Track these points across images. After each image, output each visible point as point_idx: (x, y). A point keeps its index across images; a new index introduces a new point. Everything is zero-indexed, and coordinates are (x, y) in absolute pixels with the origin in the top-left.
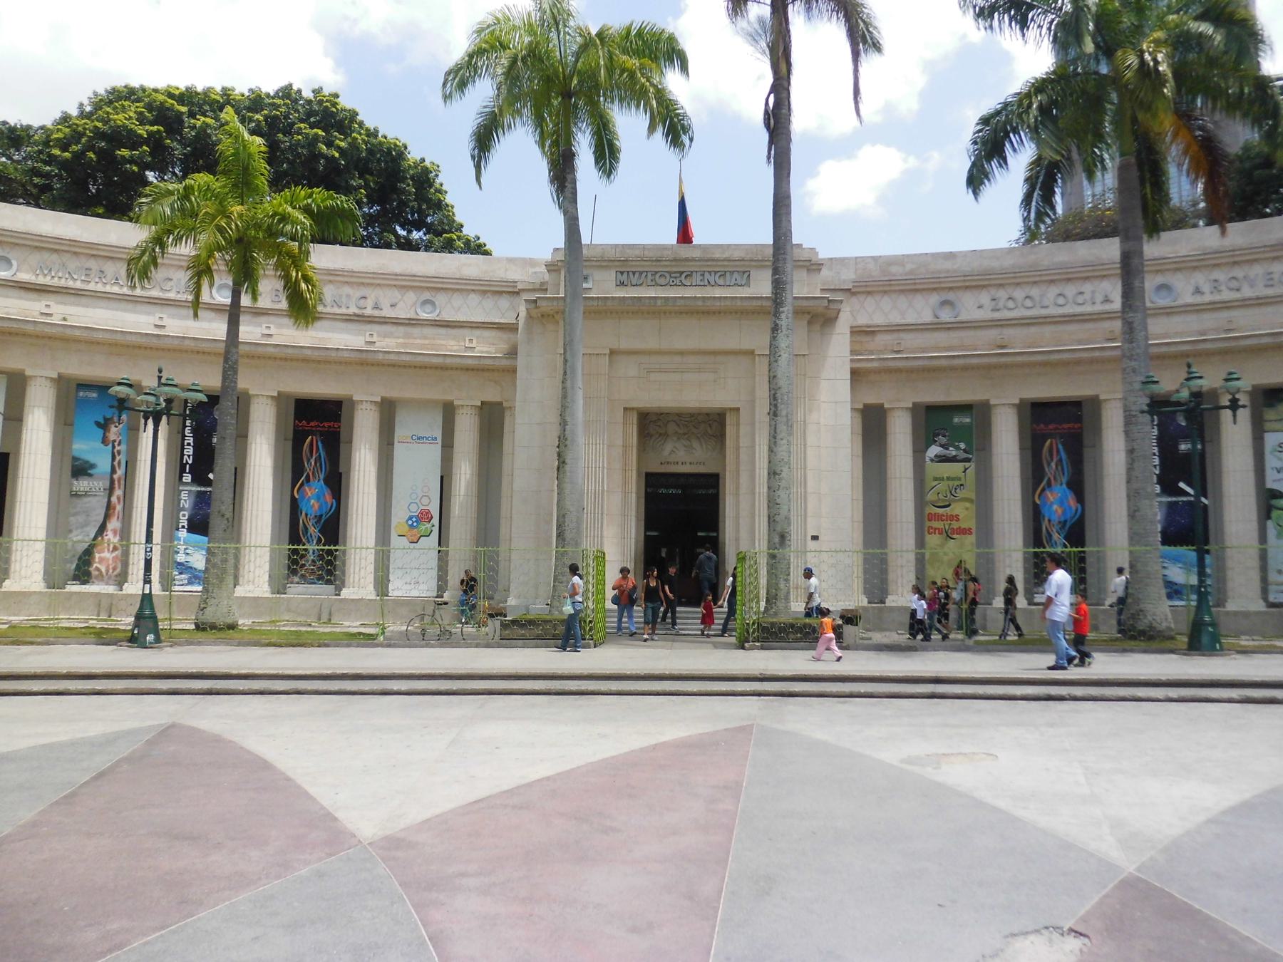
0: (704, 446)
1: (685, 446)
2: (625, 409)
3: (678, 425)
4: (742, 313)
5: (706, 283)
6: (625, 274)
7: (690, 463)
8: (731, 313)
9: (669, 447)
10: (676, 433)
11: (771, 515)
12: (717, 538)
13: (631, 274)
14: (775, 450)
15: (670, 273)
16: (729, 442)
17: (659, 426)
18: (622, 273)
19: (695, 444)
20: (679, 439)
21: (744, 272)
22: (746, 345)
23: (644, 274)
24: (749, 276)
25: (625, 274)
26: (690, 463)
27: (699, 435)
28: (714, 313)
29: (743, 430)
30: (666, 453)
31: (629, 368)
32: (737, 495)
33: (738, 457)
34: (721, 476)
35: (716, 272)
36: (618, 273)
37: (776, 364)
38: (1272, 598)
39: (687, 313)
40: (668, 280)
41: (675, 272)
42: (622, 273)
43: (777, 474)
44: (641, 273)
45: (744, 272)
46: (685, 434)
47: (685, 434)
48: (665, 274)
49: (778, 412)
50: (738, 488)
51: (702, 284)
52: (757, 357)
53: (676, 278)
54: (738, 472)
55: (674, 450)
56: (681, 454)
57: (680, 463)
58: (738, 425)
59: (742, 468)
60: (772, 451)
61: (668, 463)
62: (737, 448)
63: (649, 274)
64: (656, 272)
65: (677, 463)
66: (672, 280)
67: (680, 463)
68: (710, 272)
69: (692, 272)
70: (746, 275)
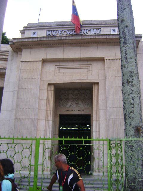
0: (84, 102)
1: (76, 103)
2: (49, 84)
3: (73, 95)
4: (98, 43)
6: (51, 31)
7: (78, 110)
8: (94, 43)
9: (69, 104)
10: (72, 98)
11: (127, 113)
12: (61, 125)
13: (53, 31)
14: (127, 65)
16: (94, 98)
17: (66, 96)
18: (49, 31)
19: (80, 103)
20: (73, 100)
21: (98, 29)
22: (101, 55)
25: (51, 31)
26: (78, 110)
27: (82, 99)
28: (86, 43)
29: (100, 91)
30: (68, 106)
31: (51, 67)
32: (98, 121)
33: (98, 104)
34: (91, 116)
35: (87, 29)
36: (48, 32)
37: (122, 14)
38: (12, 143)
39: (75, 44)
40: (67, 33)
41: (70, 30)
42: (49, 31)
43: (130, 82)
44: (57, 31)
45: (98, 29)
46: (76, 98)
47: (76, 98)
48: (67, 31)
49: (127, 41)
50: (99, 117)
52: (105, 60)
53: (70, 32)
54: (98, 110)
55: (72, 105)
56: (74, 107)
57: (74, 110)
58: (98, 90)
59: (101, 108)
60: (124, 67)
61: (69, 110)
62: (98, 100)
63: (60, 31)
64: (63, 30)
65: (73, 110)
66: (69, 33)
67: (74, 110)
69: (91, 29)
70: (99, 30)
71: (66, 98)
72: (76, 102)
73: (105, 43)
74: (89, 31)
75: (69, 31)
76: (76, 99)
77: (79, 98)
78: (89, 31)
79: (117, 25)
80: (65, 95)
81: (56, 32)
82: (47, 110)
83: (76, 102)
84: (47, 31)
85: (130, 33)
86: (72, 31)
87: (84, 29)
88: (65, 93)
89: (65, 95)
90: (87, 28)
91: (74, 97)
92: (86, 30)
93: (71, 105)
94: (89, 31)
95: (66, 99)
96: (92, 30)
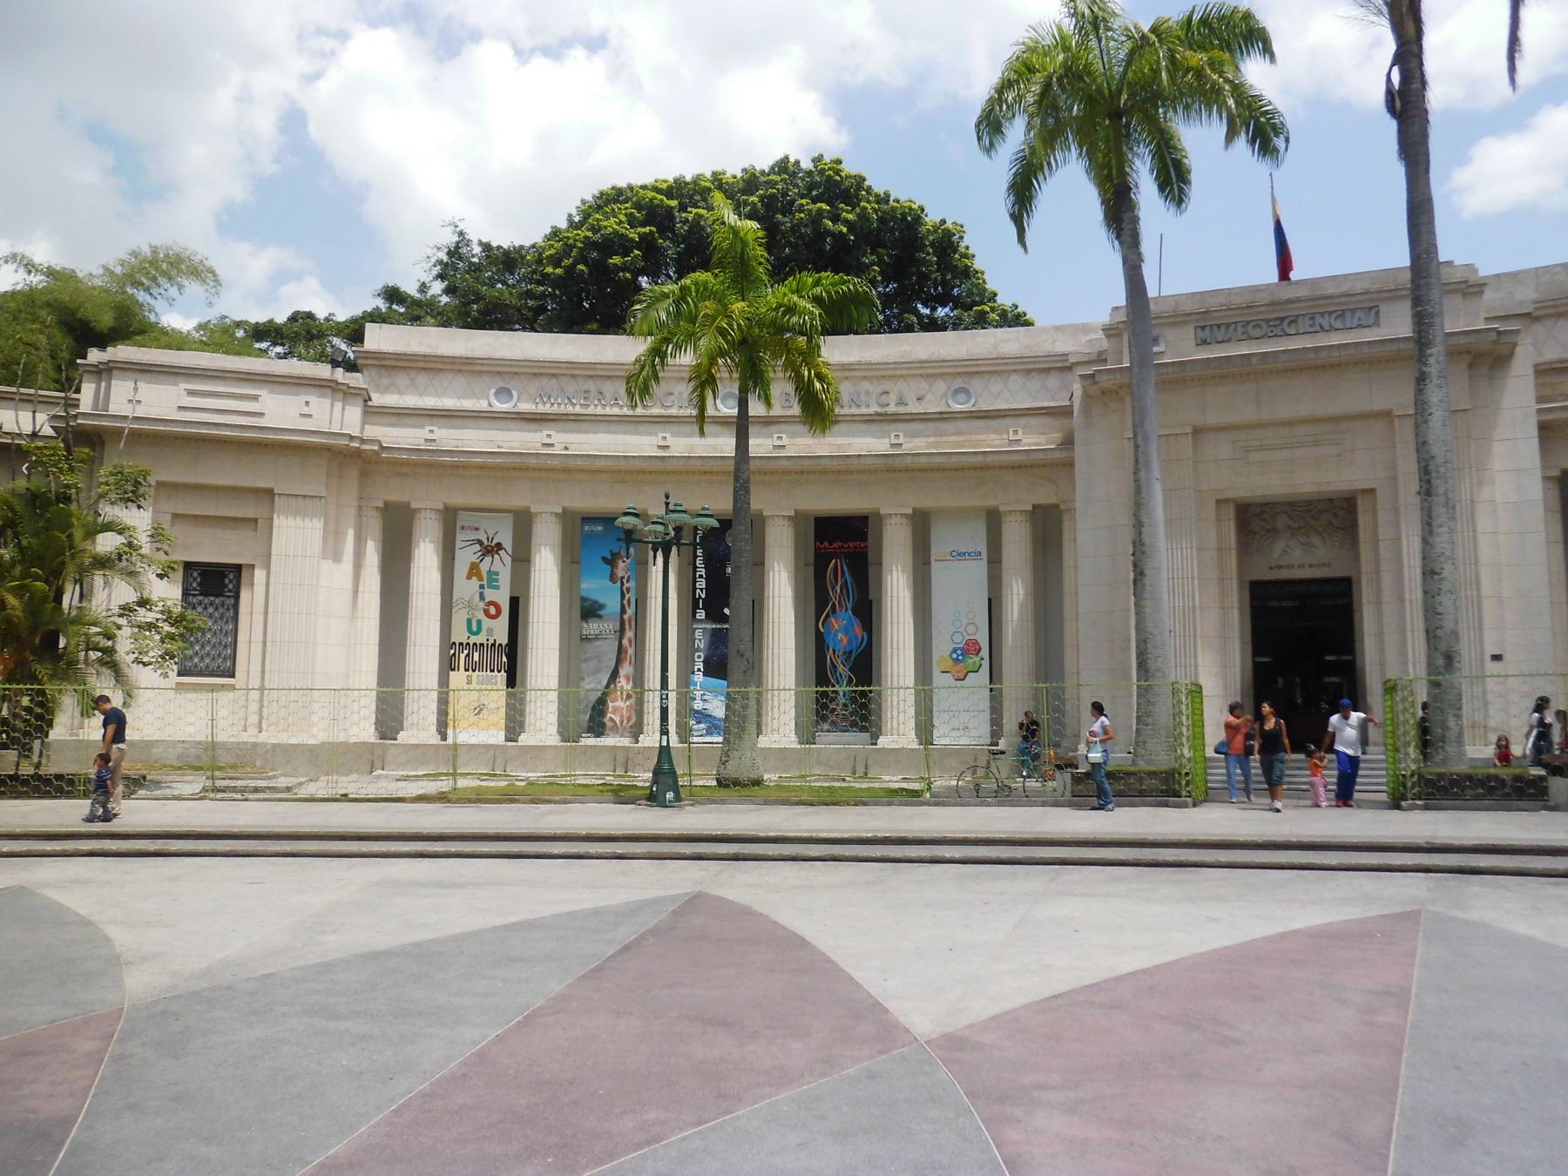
1: (1302, 544)
3: (1291, 518)
5: (1318, 329)
6: (1208, 329)
9: (1280, 545)
10: (1289, 527)
13: (1216, 330)
15: (1267, 321)
17: (1265, 520)
19: (1316, 540)
22: (1379, 404)
23: (1232, 327)
24: (1378, 312)
27: (1320, 529)
30: (1276, 554)
34: (1354, 580)
35: (1331, 313)
36: (1199, 330)
41: (1276, 319)
48: (1262, 323)
50: (1378, 594)
51: (1312, 330)
53: (1275, 326)
55: (1287, 549)
56: (1297, 555)
62: (1375, 543)
64: (1248, 323)
68: (1322, 314)
69: (1297, 316)
70: (1374, 311)
71: (1268, 527)
72: (1301, 540)
73: (1395, 360)
74: (1290, 323)
75: (1271, 323)
76: (1303, 531)
77: (1311, 527)
78: (1293, 325)
79: (1225, 778)
80: (1264, 517)
81: (1353, 317)
82: (1222, 580)
83: (1301, 540)
84: (1196, 327)
85: (490, 278)
86: (1277, 322)
87: (1322, 314)
88: (1264, 511)
89: (1264, 517)
90: (1331, 309)
91: (1291, 524)
92: (1326, 316)
93: (1285, 551)
94: (1254, 326)
95: (1268, 531)
96: (1348, 314)
